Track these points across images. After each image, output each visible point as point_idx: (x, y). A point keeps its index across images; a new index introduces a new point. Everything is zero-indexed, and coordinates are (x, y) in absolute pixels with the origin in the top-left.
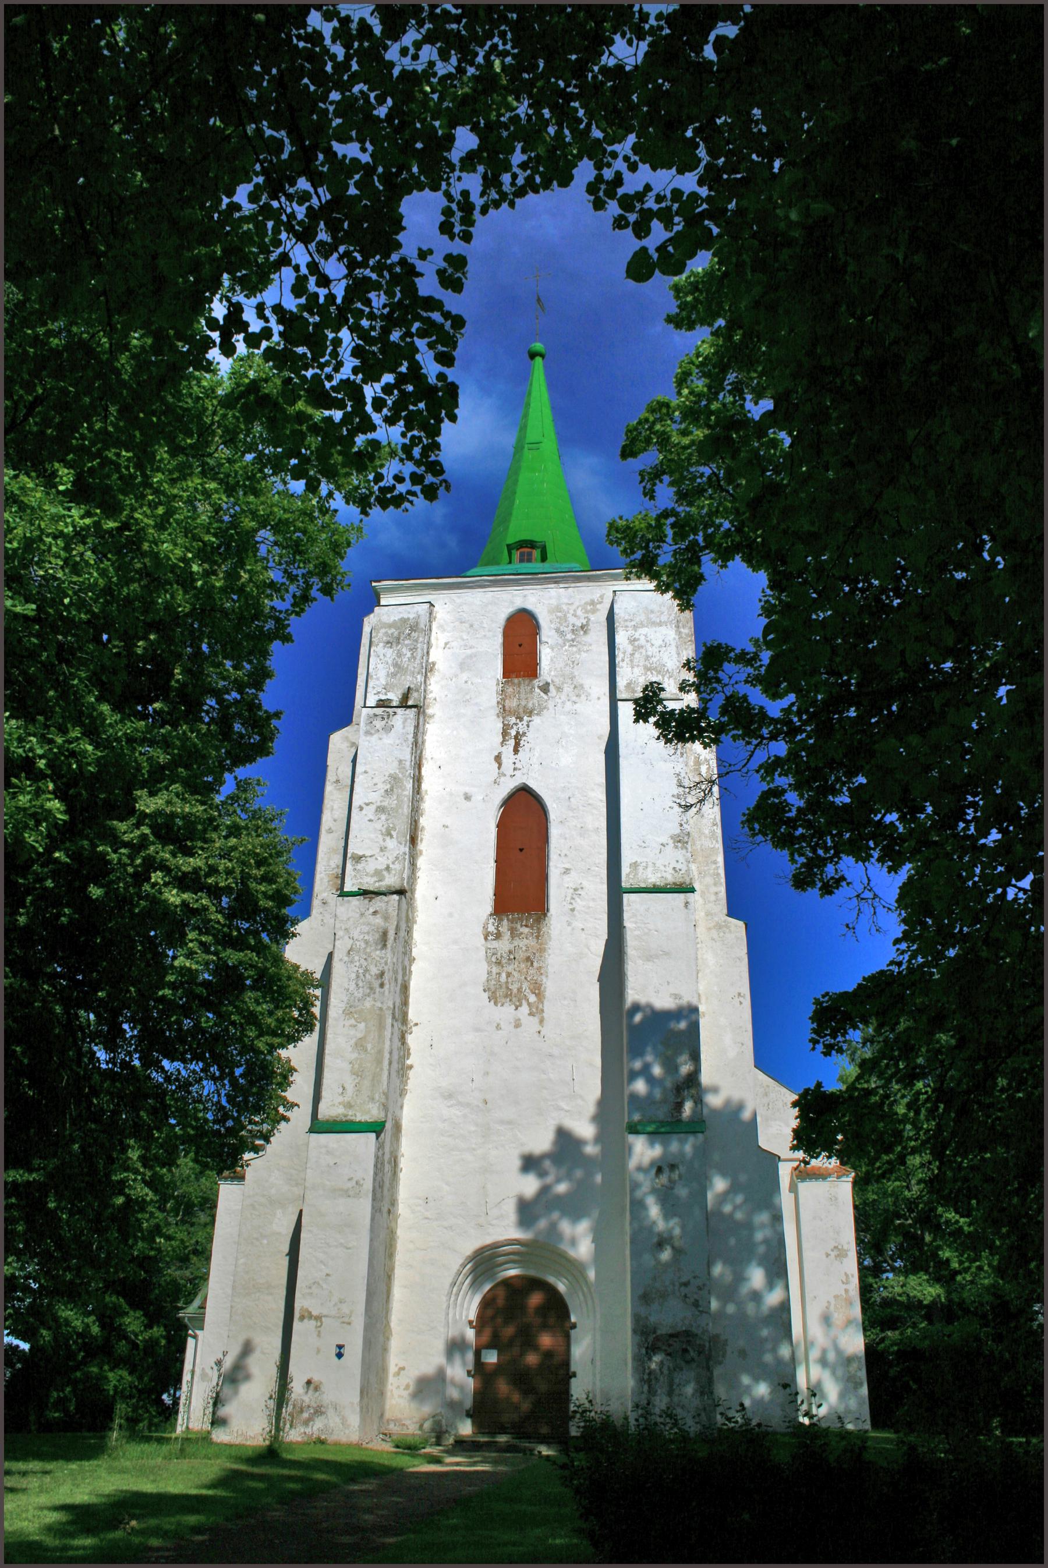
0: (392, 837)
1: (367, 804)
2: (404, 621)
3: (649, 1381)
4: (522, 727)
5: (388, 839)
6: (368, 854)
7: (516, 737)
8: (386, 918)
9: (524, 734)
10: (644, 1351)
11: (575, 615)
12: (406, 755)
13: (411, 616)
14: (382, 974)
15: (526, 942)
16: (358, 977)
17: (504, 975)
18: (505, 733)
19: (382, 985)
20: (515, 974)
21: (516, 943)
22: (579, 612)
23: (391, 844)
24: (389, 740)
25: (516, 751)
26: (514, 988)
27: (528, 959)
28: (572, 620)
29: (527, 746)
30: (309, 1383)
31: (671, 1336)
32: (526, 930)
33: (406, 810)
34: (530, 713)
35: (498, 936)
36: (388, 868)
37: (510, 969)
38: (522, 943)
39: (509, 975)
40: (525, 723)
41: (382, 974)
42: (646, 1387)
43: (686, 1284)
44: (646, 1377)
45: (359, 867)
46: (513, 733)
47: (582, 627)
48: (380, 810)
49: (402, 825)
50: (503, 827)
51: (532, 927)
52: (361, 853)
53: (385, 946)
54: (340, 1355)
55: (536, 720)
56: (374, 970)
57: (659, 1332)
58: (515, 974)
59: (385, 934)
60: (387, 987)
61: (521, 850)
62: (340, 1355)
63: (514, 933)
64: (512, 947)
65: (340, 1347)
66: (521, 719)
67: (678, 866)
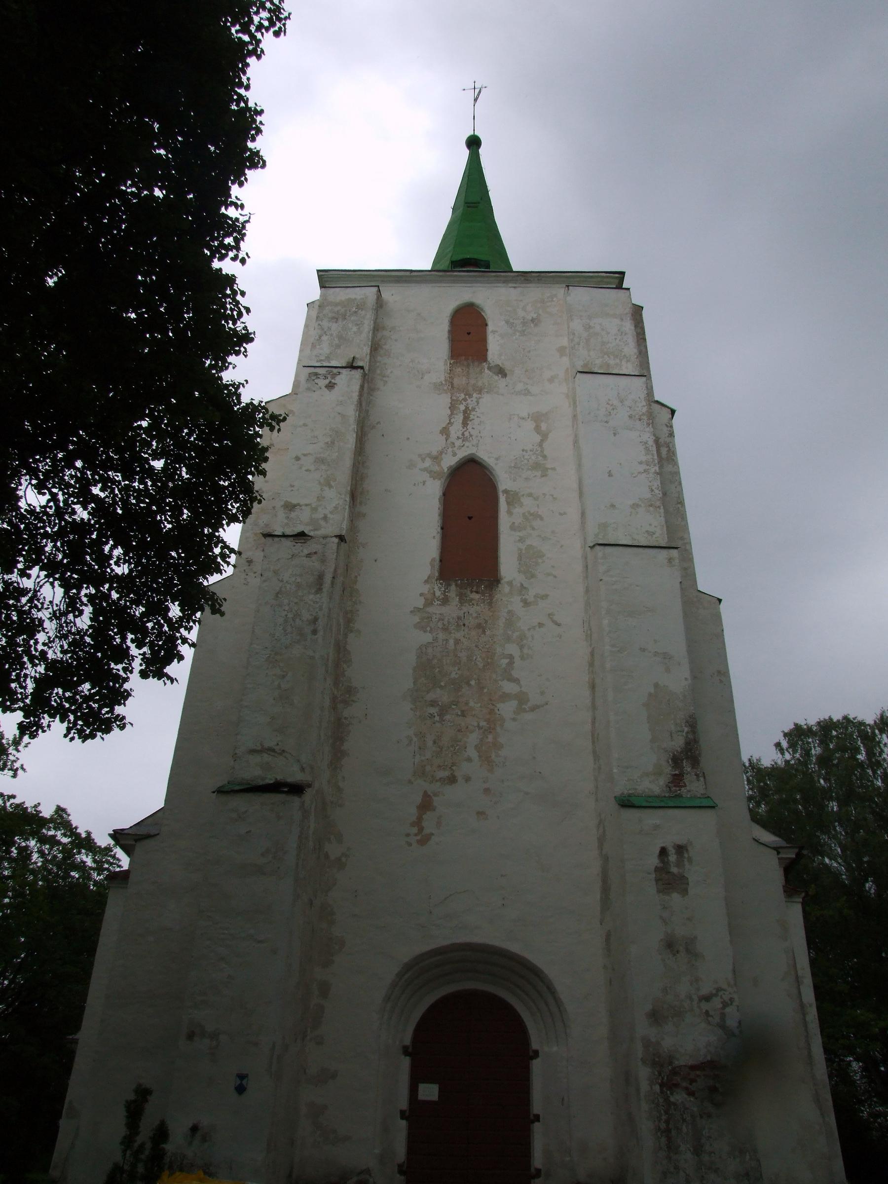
0: (330, 487)
1: (305, 455)
2: (350, 301)
3: (668, 1131)
4: (471, 403)
5: (327, 488)
6: (302, 502)
7: (465, 412)
8: (323, 561)
9: (474, 409)
10: (657, 1088)
11: (524, 309)
12: (351, 412)
13: (358, 297)
14: (315, 620)
15: (476, 609)
16: (286, 621)
17: (451, 642)
18: (453, 407)
19: (315, 632)
20: (464, 640)
21: (465, 609)
22: (529, 308)
23: (330, 494)
24: (331, 397)
25: (465, 424)
26: (463, 655)
27: (479, 626)
28: (521, 313)
29: (476, 421)
30: (194, 1129)
31: (693, 1068)
32: (476, 596)
33: (347, 462)
34: (480, 391)
35: (445, 601)
36: (325, 518)
37: (459, 635)
38: (473, 610)
39: (457, 642)
40: (474, 399)
41: (315, 620)
42: (663, 1140)
43: (707, 998)
44: (663, 1126)
45: (293, 515)
46: (462, 407)
47: (533, 320)
48: (320, 461)
49: (343, 474)
50: (448, 497)
51: (483, 594)
52: (294, 502)
53: (319, 590)
54: (241, 1089)
55: (486, 399)
56: (306, 616)
57: (167, 1172)
58: (464, 640)
59: (321, 577)
60: (321, 633)
61: (470, 518)
62: (241, 1089)
63: (462, 598)
64: (461, 614)
65: (242, 1077)
66: (471, 396)
67: (652, 529)
